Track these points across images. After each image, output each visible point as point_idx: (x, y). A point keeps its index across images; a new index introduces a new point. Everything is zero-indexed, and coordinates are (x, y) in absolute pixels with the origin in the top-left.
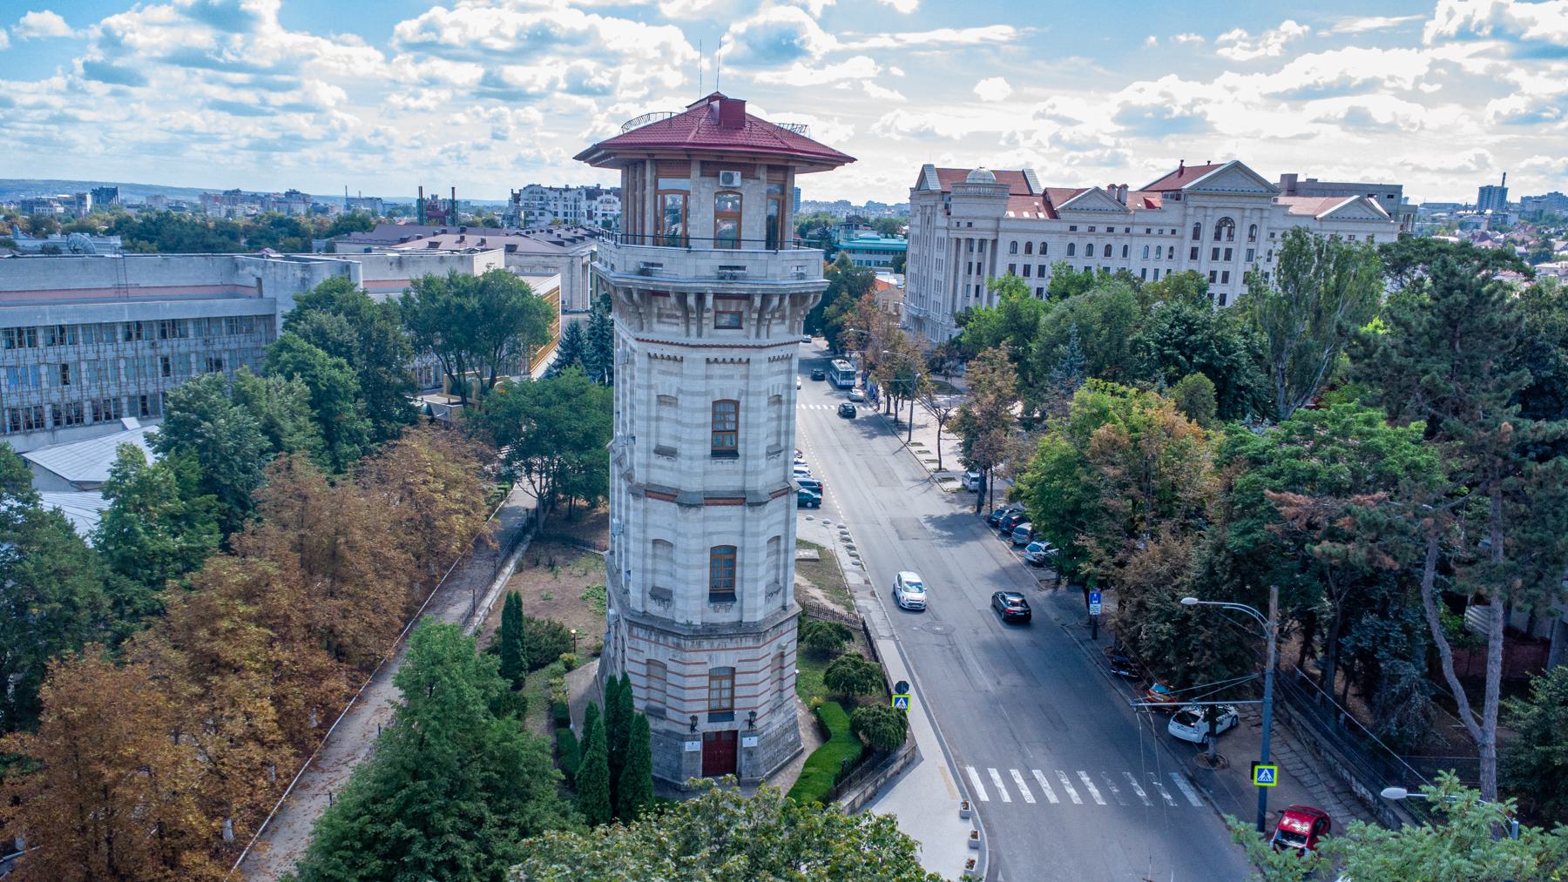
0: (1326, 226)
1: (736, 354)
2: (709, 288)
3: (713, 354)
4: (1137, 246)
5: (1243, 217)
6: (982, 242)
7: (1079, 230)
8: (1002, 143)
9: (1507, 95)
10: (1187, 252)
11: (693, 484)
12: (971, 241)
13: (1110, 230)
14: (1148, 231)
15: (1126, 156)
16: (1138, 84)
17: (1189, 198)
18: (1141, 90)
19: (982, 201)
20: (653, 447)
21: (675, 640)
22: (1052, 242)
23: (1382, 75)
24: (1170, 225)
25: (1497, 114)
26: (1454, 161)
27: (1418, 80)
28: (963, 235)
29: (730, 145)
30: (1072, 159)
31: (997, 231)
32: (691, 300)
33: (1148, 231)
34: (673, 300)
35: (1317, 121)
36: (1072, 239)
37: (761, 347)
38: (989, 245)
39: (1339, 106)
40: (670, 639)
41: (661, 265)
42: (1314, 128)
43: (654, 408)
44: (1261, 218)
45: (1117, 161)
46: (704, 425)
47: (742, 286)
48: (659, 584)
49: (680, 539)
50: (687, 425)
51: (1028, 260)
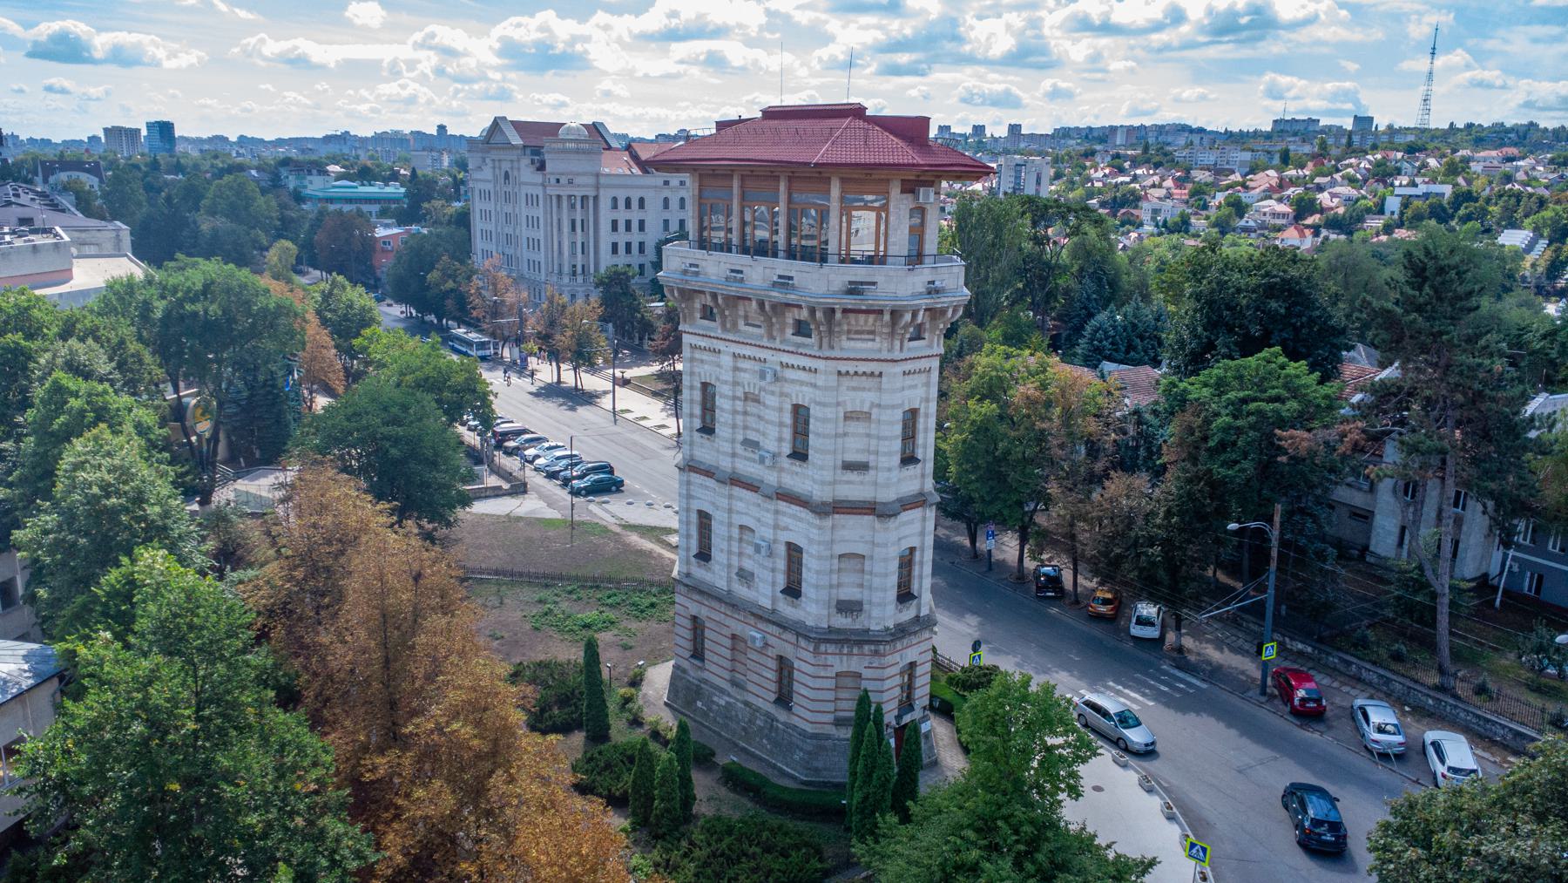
6: (584, 198)
8: (385, 74)
9: (826, 45)
11: (887, 495)
12: (559, 197)
15: (513, 91)
16: (514, 20)
18: (519, 25)
19: (582, 157)
20: (839, 463)
21: (873, 647)
22: (649, 196)
23: (731, 22)
25: (820, 60)
27: (761, 28)
28: (564, 192)
29: (951, 165)
30: (457, 91)
31: (597, 187)
34: (754, 304)
35: (682, 62)
36: (666, 193)
39: (700, 47)
40: (866, 648)
41: (874, 283)
42: (682, 68)
43: (841, 424)
45: (503, 96)
46: (896, 437)
47: (943, 300)
48: (842, 597)
49: (877, 550)
50: (886, 438)
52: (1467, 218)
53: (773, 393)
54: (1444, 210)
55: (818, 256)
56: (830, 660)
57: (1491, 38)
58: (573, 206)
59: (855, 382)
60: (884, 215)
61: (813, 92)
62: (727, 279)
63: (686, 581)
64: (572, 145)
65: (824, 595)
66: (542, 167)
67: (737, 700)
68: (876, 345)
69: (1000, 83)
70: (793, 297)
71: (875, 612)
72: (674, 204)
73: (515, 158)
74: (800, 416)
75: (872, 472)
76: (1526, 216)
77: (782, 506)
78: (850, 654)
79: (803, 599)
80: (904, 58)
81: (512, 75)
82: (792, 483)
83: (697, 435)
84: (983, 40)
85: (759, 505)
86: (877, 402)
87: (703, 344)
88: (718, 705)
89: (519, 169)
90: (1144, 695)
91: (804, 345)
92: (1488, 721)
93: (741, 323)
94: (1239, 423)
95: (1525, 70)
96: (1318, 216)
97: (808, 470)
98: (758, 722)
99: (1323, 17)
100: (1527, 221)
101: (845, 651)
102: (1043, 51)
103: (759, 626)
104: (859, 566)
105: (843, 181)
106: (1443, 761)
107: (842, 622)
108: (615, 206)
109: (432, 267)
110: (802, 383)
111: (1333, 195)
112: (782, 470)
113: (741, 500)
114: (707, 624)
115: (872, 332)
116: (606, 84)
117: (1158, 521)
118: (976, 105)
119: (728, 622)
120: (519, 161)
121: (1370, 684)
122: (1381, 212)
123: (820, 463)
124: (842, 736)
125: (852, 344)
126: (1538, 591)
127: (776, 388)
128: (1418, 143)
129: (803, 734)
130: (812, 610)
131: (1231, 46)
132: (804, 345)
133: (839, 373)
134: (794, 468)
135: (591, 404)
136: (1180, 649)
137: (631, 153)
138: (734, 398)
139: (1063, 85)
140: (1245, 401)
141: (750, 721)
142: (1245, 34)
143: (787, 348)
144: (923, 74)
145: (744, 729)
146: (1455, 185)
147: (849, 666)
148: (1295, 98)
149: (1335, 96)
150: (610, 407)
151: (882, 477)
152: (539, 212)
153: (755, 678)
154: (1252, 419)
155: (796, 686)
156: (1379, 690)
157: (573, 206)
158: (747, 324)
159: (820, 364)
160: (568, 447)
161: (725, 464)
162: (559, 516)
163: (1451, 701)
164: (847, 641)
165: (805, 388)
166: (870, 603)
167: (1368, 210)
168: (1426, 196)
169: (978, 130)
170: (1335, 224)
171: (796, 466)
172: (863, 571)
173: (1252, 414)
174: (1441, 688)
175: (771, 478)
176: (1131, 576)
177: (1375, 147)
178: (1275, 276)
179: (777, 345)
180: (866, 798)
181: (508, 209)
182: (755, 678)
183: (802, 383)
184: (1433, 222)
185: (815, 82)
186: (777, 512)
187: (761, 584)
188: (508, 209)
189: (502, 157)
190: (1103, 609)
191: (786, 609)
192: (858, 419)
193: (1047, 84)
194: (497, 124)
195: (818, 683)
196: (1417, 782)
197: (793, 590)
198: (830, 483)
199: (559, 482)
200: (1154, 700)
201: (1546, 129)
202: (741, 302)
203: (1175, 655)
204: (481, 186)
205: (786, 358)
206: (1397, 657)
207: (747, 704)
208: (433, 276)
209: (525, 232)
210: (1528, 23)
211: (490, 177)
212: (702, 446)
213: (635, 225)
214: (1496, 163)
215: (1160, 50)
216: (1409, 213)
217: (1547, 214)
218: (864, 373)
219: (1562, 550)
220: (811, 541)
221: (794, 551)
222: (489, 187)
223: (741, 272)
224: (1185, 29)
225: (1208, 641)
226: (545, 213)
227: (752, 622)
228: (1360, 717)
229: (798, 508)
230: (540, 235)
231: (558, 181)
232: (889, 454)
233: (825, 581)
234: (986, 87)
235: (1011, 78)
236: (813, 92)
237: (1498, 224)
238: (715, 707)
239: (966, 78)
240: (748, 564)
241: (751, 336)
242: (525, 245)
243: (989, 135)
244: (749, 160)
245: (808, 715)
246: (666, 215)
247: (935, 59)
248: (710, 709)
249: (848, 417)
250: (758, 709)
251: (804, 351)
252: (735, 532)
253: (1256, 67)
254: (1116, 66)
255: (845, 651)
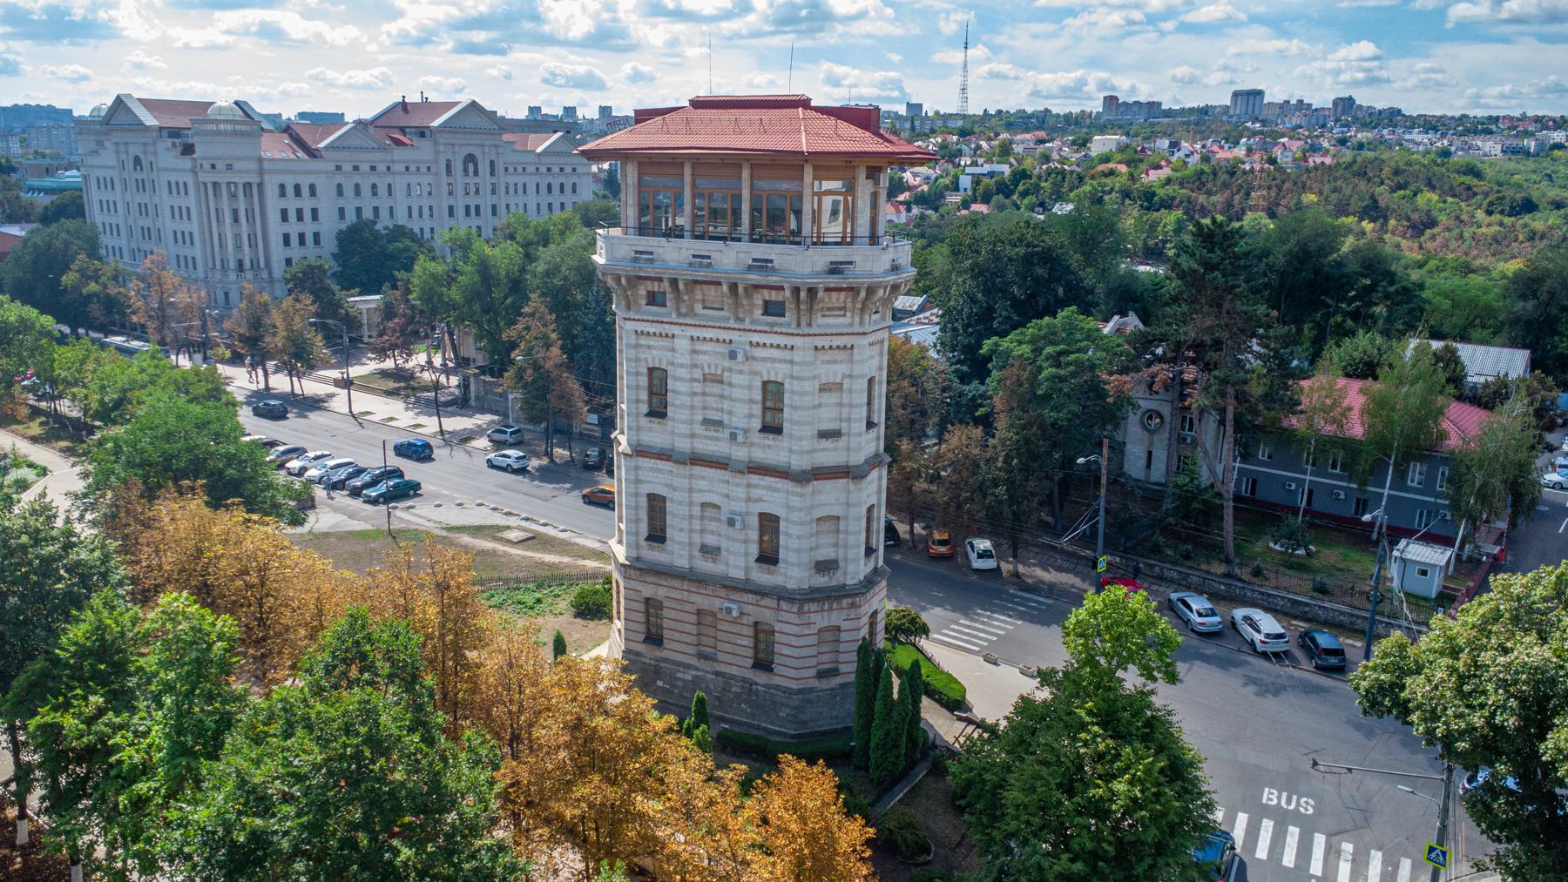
0: (544, 160)
1: (837, 341)
2: (821, 282)
3: (820, 342)
4: (400, 183)
5: (483, 153)
6: (247, 186)
7: (379, 169)
10: (445, 189)
12: (215, 184)
13: (373, 168)
14: (407, 169)
17: (438, 135)
21: (850, 601)
24: (425, 162)
25: (389, 34)
26: (362, 76)
28: (222, 179)
31: (261, 172)
32: (803, 295)
33: (407, 169)
35: (229, 32)
36: (339, 179)
37: (864, 334)
38: (255, 189)
40: (845, 602)
41: (851, 263)
42: (231, 39)
43: (817, 396)
44: (454, 153)
49: (851, 509)
51: (299, 203)
52: (1024, 194)
53: (741, 372)
54: (1007, 187)
55: (795, 238)
56: (813, 617)
57: (1000, 34)
58: (233, 196)
59: (829, 355)
60: (850, 198)
61: (385, 69)
62: (690, 264)
63: (638, 565)
64: (229, 127)
65: (805, 558)
66: (188, 150)
67: (707, 672)
68: (847, 320)
69: (581, 64)
70: (775, 278)
71: (851, 568)
72: (349, 191)
73: (150, 140)
74: (772, 394)
75: (844, 438)
76: (1071, 190)
77: (754, 479)
78: (831, 609)
79: (781, 565)
80: (480, 36)
81: (18, 45)
82: (764, 456)
83: (644, 421)
84: (562, 21)
85: (728, 482)
86: (848, 373)
87: (652, 330)
88: (683, 680)
89: (155, 153)
90: (1010, 616)
91: (780, 325)
92: (1270, 595)
93: (698, 308)
94: (1062, 372)
95: (1030, 63)
96: (907, 194)
97: (783, 442)
98: (734, 689)
99: (873, 14)
100: (1072, 195)
101: (826, 607)
102: (622, 33)
103: (732, 597)
104: (833, 527)
105: (815, 168)
106: (1259, 632)
107: (821, 581)
108: (283, 194)
109: (66, 268)
110: (774, 360)
111: (915, 175)
112: (752, 444)
113: (703, 478)
114: (665, 604)
115: (844, 309)
116: (139, 56)
117: (999, 465)
118: (560, 86)
119: (693, 598)
120: (155, 144)
121: (1171, 581)
122: (957, 189)
123: (798, 434)
124: (824, 687)
125: (826, 320)
126: (1253, 492)
127: (746, 368)
128: (969, 128)
129: (788, 691)
130: (793, 572)
131: (792, 36)
132: (780, 325)
133: (816, 348)
134: (766, 442)
135: (320, 408)
136: (1017, 575)
137: (291, 136)
138: (693, 380)
139: (645, 69)
140: (1060, 353)
141: (724, 689)
142: (804, 26)
143: (759, 328)
144: (503, 52)
145: (718, 698)
146: (1011, 165)
147: (829, 621)
148: (851, 86)
149: (883, 84)
150: (346, 410)
151: (854, 442)
152: (191, 201)
153: (727, 647)
154: (1072, 368)
155: (777, 648)
156: (1179, 585)
157: (233, 196)
158: (704, 308)
159: (797, 341)
160: (656, 435)
161: (683, 445)
162: (370, 527)
163: (1239, 584)
164: (828, 598)
165: (777, 365)
166: (846, 560)
167: (946, 188)
168: (991, 174)
169: (570, 111)
170: (921, 200)
171: (770, 440)
172: (837, 531)
173: (1071, 364)
174: (1228, 575)
175: (739, 453)
176: (980, 514)
177: (933, 131)
178: (1035, 246)
179: (747, 325)
180: (887, 734)
181: (143, 198)
182: (727, 647)
183: (774, 360)
184: (1001, 197)
185: (385, 58)
186: (749, 485)
187: (732, 558)
188: (143, 198)
189: (130, 140)
190: (943, 549)
191: (762, 577)
192: (830, 390)
193: (627, 68)
194: (119, 101)
195: (802, 642)
196: (1239, 651)
197: (768, 557)
198: (809, 452)
199: (345, 493)
200: (1020, 619)
201: (1058, 115)
202: (698, 287)
203: (1015, 580)
204: (101, 173)
205: (756, 338)
206: (1187, 556)
207: (718, 674)
208: (68, 279)
209: (168, 225)
210: (1028, 21)
211: (114, 163)
212: (650, 430)
213: (307, 215)
214: (1032, 145)
215: (730, 38)
216: (981, 188)
217: (1087, 188)
218: (838, 347)
219: (1270, 457)
220: (789, 508)
221: (769, 524)
222: (109, 174)
223: (709, 257)
224: (752, 18)
225: (1034, 565)
226: (199, 201)
227: (723, 595)
228: (1182, 606)
229: (773, 479)
230: (194, 227)
231: (213, 166)
232: (859, 420)
233: (805, 544)
234: (568, 69)
235: (589, 59)
236: (385, 69)
237: (1050, 197)
238: (679, 683)
239: (547, 59)
240: (711, 540)
241: (713, 318)
242: (171, 239)
243: (581, 117)
245: (793, 673)
246: (341, 203)
247: (514, 38)
248: (675, 686)
249: (824, 389)
250: (733, 677)
251: (779, 330)
252: (697, 511)
253: (815, 56)
254: (693, 52)
255: (826, 607)
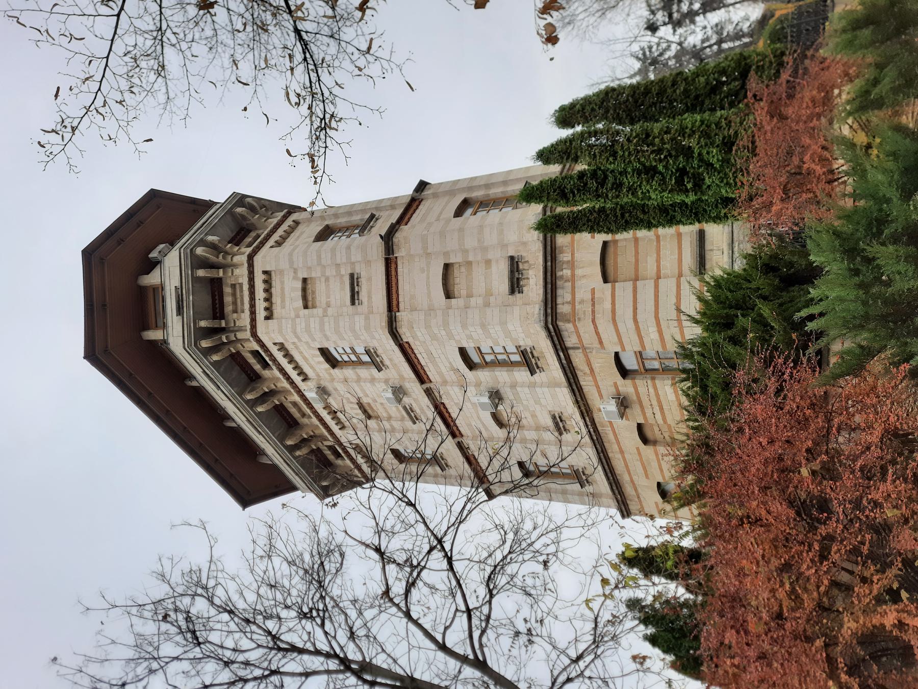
56: (583, 294)
78: (572, 265)
110: (301, 353)
133: (267, 318)
183: (301, 353)
244: (235, 405)
